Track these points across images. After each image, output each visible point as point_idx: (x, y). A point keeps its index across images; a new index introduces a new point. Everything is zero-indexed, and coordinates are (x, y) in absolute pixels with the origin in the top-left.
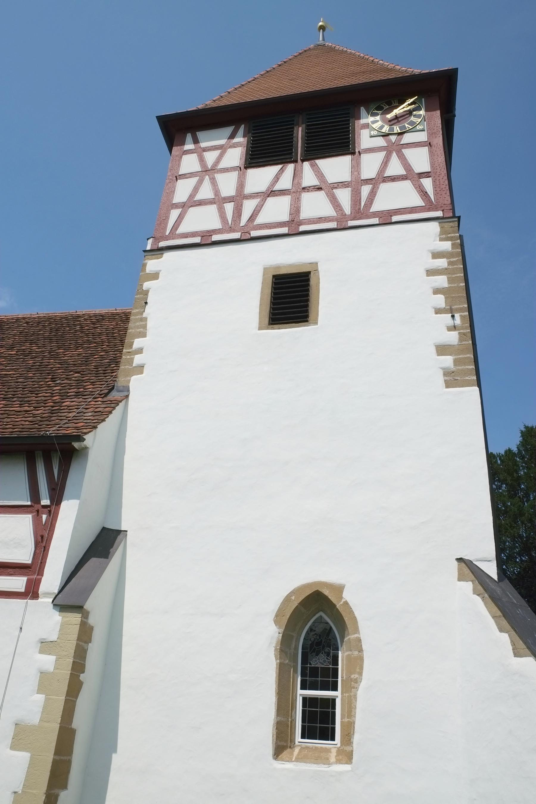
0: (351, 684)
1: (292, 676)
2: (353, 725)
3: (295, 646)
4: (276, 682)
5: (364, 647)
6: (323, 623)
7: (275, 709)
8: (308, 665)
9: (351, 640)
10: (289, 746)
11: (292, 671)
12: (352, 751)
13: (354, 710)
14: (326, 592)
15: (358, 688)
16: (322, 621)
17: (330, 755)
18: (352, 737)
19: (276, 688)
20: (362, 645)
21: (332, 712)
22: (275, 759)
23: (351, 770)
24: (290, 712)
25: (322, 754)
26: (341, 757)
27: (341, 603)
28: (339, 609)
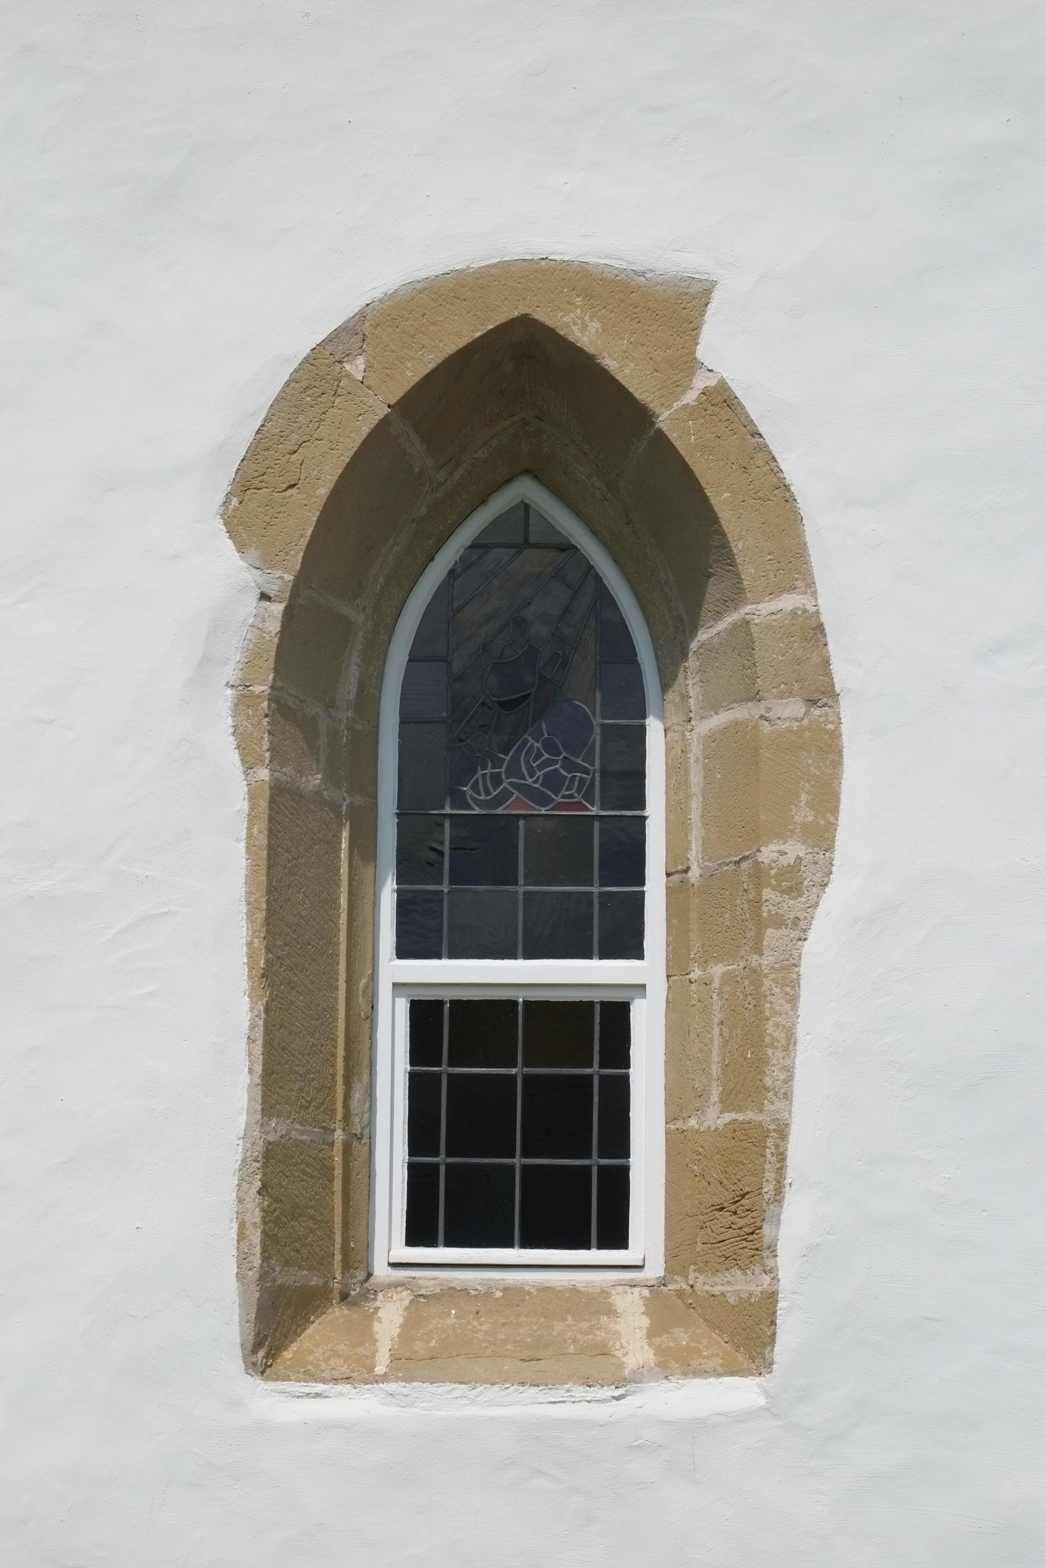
0: (758, 902)
1: (344, 870)
2: (777, 1147)
3: (361, 686)
4: (249, 903)
5: (842, 672)
6: (537, 546)
7: (251, 1071)
8: (443, 807)
9: (754, 629)
10: (336, 1292)
11: (344, 845)
12: (771, 1297)
13: (780, 1054)
14: (584, 327)
15: (802, 924)
16: (532, 539)
17: (611, 1326)
18: (768, 1215)
19: (249, 944)
20: (827, 663)
21: (603, 1079)
22: (263, 1373)
23: (765, 1409)
24: (340, 1087)
25: (558, 1326)
26: (682, 1337)
27: (690, 397)
28: (673, 436)
